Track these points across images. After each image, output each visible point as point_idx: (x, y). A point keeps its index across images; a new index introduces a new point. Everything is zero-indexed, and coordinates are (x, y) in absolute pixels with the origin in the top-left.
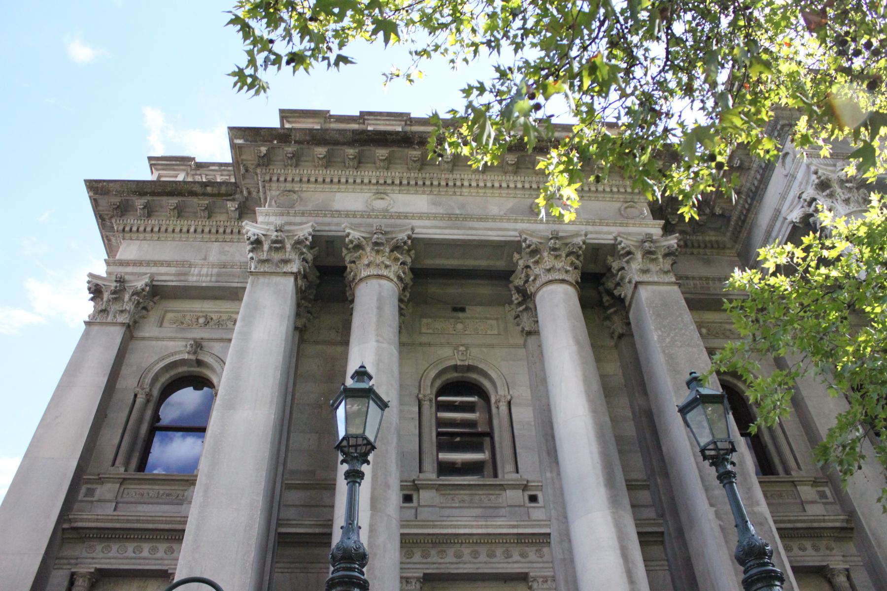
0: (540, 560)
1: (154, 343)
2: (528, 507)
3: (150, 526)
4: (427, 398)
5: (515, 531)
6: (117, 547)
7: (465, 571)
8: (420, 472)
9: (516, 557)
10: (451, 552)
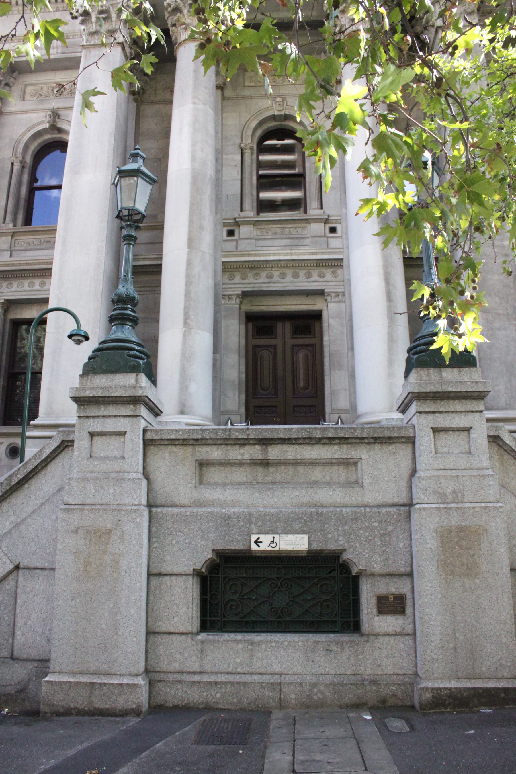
0: (334, 279)
1: (19, 116)
2: (328, 238)
3: (37, 267)
4: (248, 147)
5: (314, 257)
6: (17, 283)
7: (275, 289)
8: (241, 211)
9: (315, 277)
10: (264, 274)
